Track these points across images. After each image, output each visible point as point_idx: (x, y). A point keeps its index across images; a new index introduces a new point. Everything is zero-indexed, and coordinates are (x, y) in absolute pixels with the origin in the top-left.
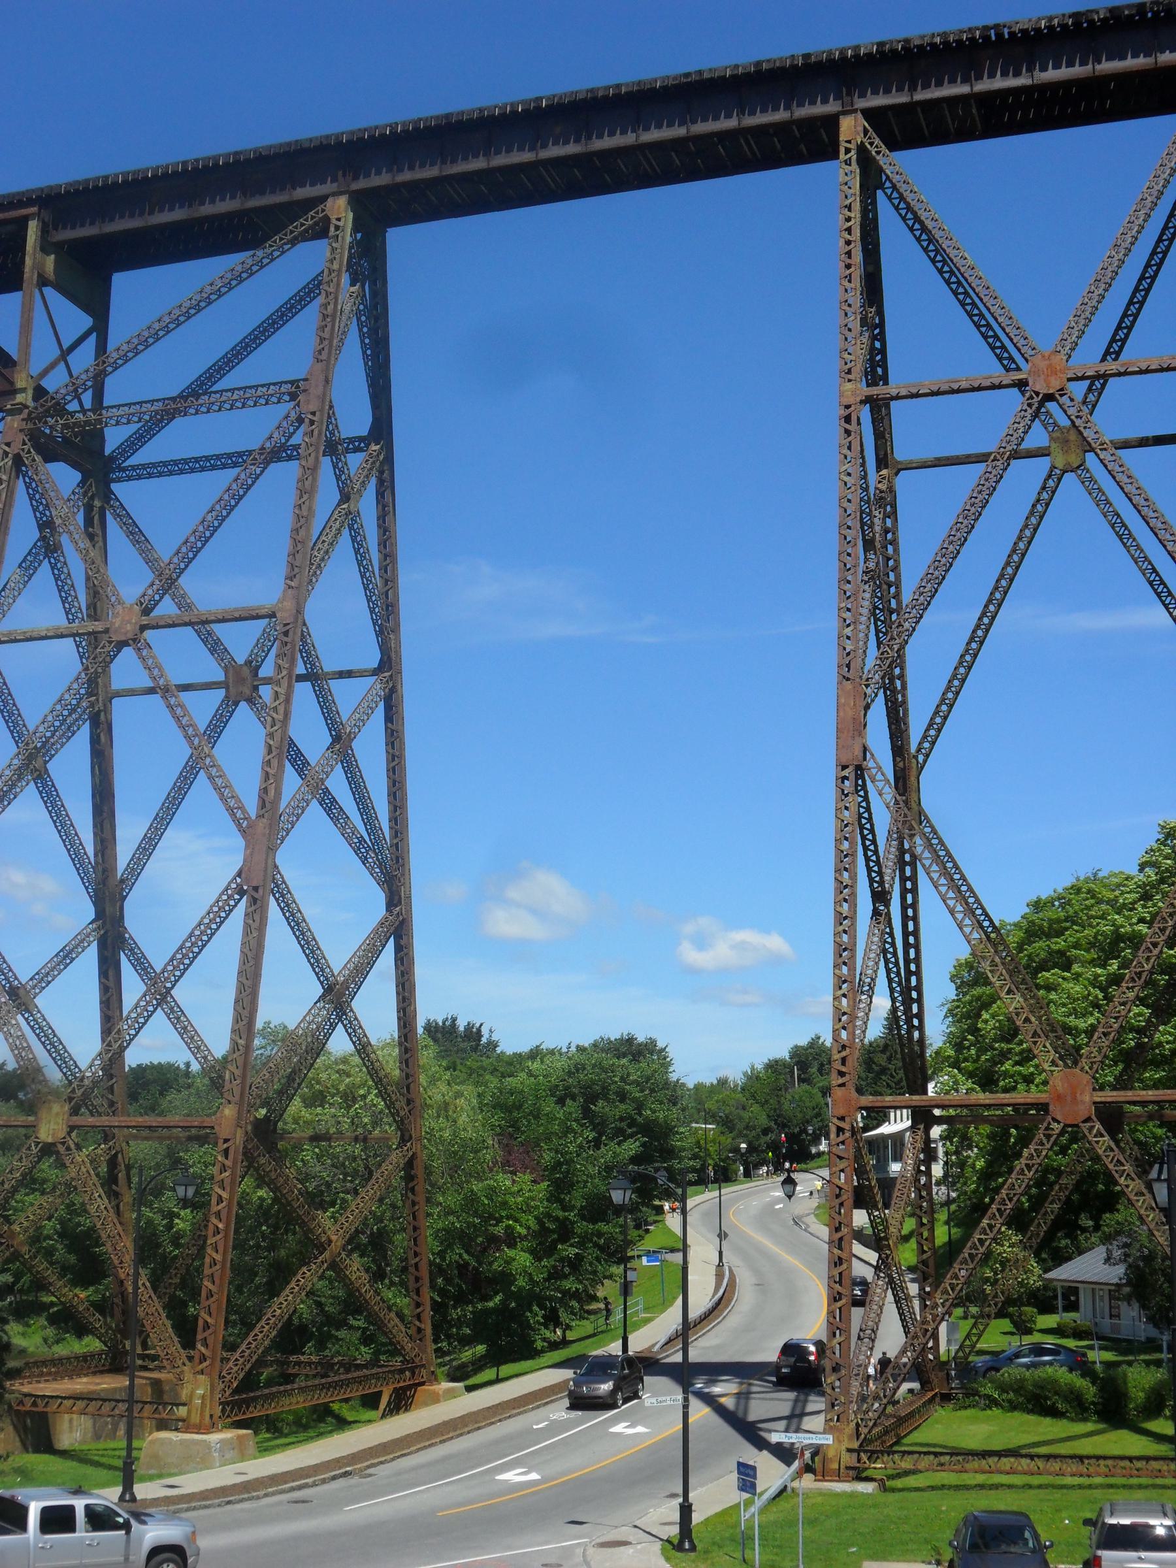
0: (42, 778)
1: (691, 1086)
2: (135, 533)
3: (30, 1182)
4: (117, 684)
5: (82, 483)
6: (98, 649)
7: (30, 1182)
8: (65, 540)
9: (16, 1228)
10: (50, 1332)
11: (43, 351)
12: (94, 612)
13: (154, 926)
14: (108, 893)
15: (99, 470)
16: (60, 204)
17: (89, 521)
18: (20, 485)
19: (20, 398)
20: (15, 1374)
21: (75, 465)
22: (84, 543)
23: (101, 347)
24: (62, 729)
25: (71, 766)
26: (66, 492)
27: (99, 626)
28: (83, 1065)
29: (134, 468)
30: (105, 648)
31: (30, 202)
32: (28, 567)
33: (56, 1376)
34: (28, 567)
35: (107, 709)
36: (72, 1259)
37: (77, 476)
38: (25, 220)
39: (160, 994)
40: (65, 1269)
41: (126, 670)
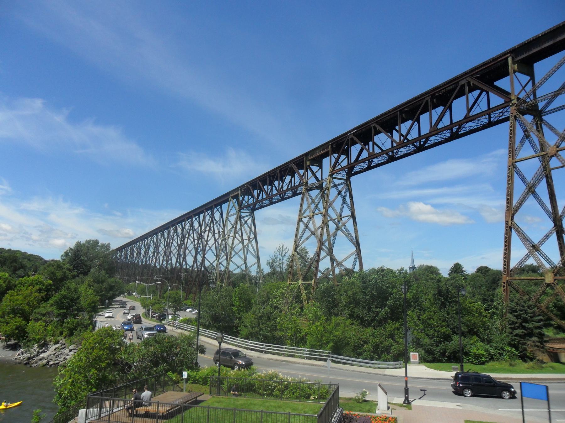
0: (534, 193)
2: (551, 128)
3: (544, 293)
4: (551, 167)
5: (534, 118)
6: (545, 159)
7: (544, 293)
8: (531, 134)
9: (542, 305)
10: (555, 331)
11: (518, 88)
12: (542, 150)
15: (538, 114)
16: (515, 52)
17: (537, 128)
18: (517, 123)
19: (513, 102)
20: (547, 342)
21: (531, 114)
22: (537, 133)
23: (534, 83)
24: (538, 180)
25: (542, 189)
26: (530, 122)
27: (544, 153)
28: (556, 263)
29: (548, 111)
30: (547, 158)
31: (508, 53)
32: (522, 142)
33: (559, 343)
34: (522, 142)
35: (550, 173)
36: (559, 313)
37: (532, 117)
38: (507, 58)
40: (557, 316)
41: (554, 163)
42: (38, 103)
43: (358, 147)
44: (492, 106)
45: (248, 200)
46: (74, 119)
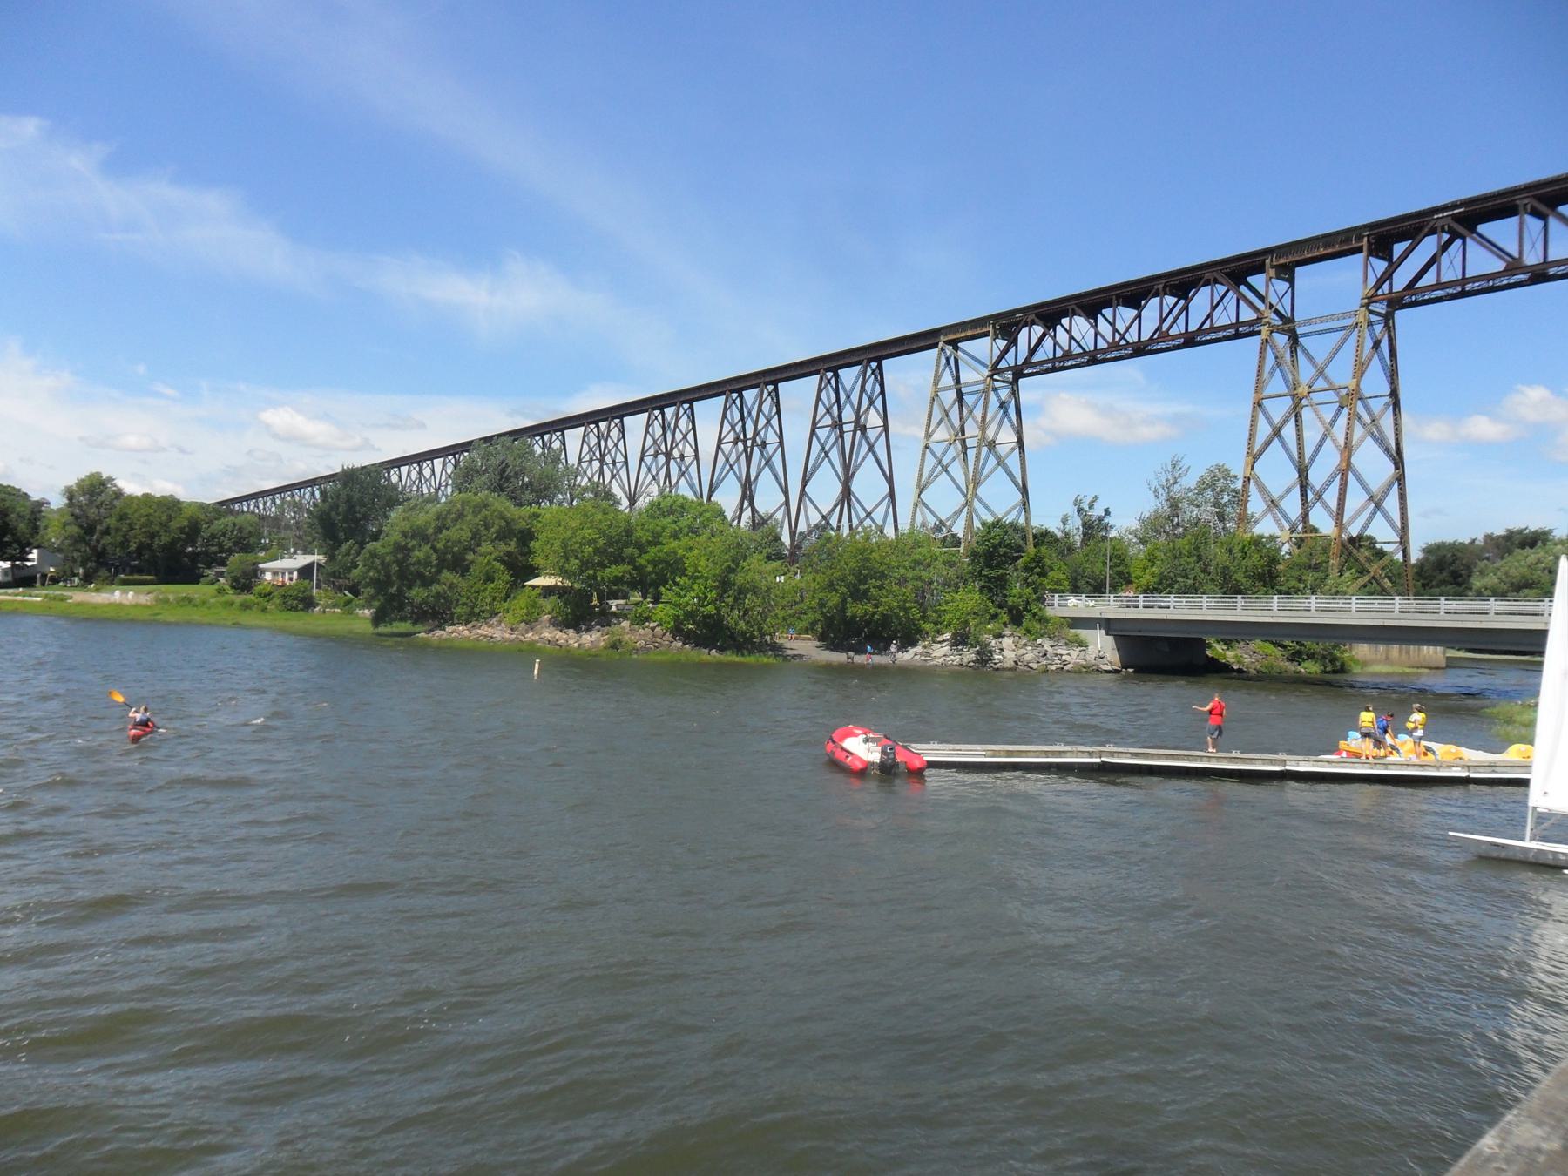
1: (57, 502)
13: (1316, 477)
14: (1303, 472)
25: (1289, 431)
33: (189, 1049)
39: (1319, 497)
42: (30, 126)
43: (1034, 332)
44: (1550, 259)
45: (1113, 325)
46: (118, 166)
